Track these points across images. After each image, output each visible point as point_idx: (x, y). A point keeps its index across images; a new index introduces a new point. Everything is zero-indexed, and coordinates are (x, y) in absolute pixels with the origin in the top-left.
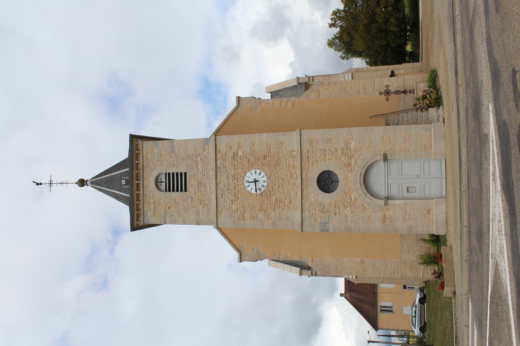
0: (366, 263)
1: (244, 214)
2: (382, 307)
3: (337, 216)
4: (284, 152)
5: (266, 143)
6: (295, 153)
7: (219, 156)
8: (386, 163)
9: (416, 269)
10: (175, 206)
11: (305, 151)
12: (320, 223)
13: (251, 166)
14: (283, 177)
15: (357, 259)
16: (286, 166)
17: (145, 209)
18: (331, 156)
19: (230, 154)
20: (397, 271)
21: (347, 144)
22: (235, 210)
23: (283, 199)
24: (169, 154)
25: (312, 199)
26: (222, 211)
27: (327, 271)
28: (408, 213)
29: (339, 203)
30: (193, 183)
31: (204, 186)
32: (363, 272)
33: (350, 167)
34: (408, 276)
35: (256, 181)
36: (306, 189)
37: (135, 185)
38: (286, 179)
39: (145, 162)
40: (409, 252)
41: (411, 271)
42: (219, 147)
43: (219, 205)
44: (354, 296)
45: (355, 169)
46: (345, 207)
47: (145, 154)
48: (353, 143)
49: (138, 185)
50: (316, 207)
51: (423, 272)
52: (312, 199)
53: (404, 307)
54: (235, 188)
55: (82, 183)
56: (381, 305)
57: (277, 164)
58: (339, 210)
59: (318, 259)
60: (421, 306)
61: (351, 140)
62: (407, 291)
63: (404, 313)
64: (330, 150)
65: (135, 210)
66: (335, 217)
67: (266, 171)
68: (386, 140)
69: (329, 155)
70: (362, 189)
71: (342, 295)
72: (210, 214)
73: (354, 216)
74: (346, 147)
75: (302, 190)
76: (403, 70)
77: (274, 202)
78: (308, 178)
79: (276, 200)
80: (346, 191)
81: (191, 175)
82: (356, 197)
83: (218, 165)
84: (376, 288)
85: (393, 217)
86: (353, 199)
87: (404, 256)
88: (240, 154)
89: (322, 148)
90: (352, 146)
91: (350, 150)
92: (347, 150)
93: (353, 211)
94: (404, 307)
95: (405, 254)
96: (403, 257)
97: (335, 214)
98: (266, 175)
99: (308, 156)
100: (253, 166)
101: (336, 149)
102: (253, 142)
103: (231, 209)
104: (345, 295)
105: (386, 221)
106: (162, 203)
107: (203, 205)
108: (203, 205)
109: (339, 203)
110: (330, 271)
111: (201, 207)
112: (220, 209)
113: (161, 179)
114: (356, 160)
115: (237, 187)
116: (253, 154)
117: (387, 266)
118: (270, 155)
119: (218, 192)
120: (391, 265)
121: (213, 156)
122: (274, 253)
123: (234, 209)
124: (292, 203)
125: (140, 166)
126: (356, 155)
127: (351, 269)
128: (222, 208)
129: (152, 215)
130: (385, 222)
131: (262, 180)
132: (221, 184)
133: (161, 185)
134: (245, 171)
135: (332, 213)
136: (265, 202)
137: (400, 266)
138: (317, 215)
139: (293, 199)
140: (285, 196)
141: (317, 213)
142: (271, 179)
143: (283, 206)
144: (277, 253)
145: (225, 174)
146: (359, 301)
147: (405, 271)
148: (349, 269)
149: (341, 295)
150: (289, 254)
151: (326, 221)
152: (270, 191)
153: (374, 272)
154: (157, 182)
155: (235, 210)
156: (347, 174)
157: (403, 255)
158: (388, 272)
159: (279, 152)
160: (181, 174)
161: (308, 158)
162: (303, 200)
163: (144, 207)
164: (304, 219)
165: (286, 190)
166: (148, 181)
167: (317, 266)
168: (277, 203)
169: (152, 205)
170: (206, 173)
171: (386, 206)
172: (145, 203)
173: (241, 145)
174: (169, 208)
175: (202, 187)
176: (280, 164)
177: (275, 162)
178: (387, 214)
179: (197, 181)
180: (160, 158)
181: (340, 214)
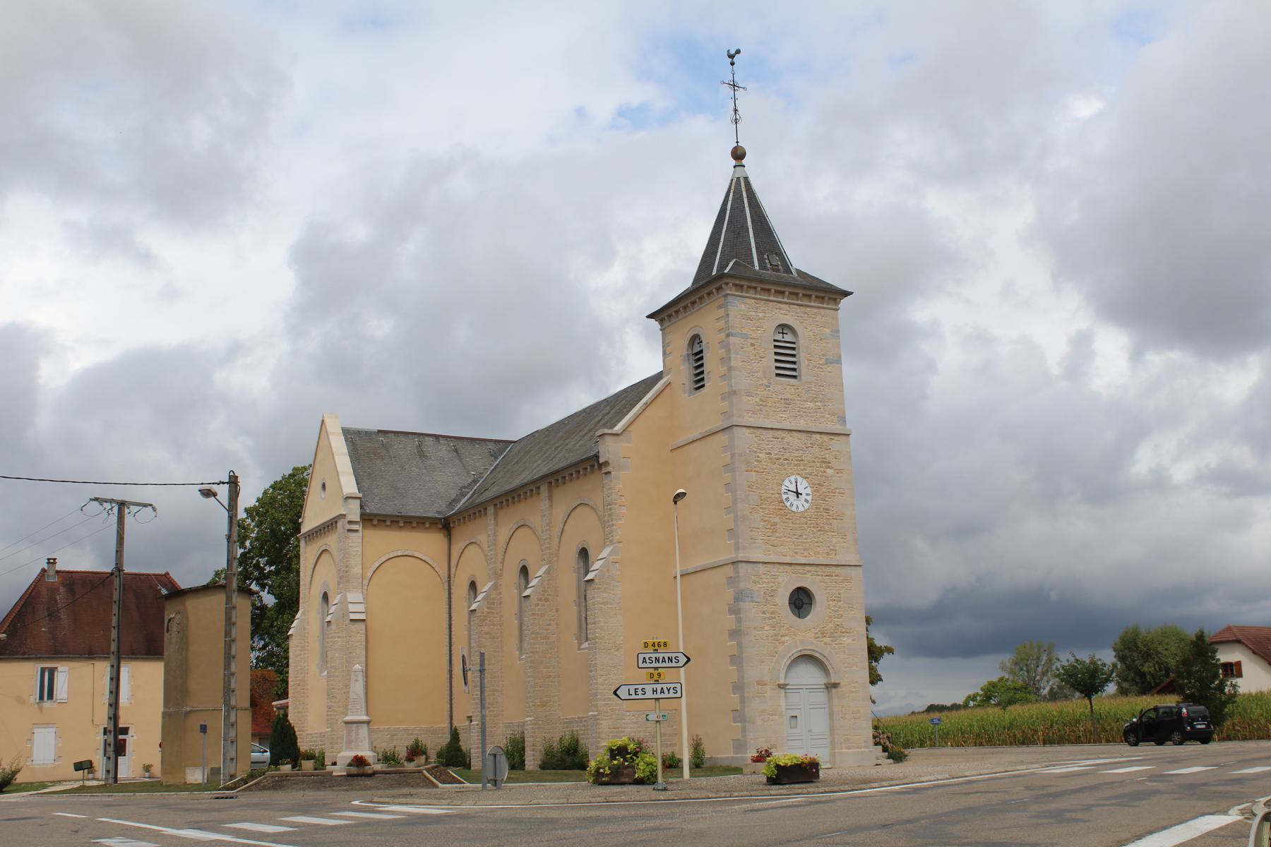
1: (755, 471)
2: (52, 671)
4: (834, 540)
6: (833, 556)
7: (826, 438)
8: (824, 686)
10: (755, 356)
11: (838, 571)
13: (816, 487)
14: (804, 536)
15: (622, 638)
16: (817, 542)
17: (749, 301)
19: (829, 457)
21: (847, 632)
22: (758, 457)
24: (824, 355)
25: (780, 579)
29: (777, 618)
30: (788, 390)
31: (785, 409)
33: (821, 636)
34: (601, 722)
35: (798, 494)
37: (783, 289)
38: (800, 540)
39: (813, 309)
41: (609, 728)
42: (836, 438)
43: (764, 432)
44: (58, 598)
46: (773, 627)
47: (822, 311)
49: (782, 293)
50: (771, 584)
52: (780, 579)
53: (54, 730)
54: (786, 459)
55: (738, 154)
56: (59, 669)
57: (819, 529)
58: (769, 619)
59: (618, 573)
60: (265, 762)
62: (98, 738)
63: (36, 730)
64: (840, 607)
65: (749, 284)
67: (811, 510)
68: (855, 688)
69: (834, 606)
70: (797, 652)
71: (52, 562)
73: (762, 639)
74: (844, 630)
75: (791, 564)
76: (533, 720)
77: (773, 520)
78: (805, 574)
79: (775, 524)
81: (798, 389)
83: (814, 436)
84: (137, 658)
85: (764, 696)
86: (783, 639)
88: (830, 472)
89: (842, 596)
90: (845, 639)
91: (841, 636)
92: (841, 632)
93: (770, 638)
94: (54, 730)
97: (764, 613)
98: (806, 511)
99: (832, 576)
100: (815, 491)
101: (842, 615)
102: (843, 493)
103: (759, 451)
104: (52, 573)
106: (759, 332)
107: (761, 405)
108: (761, 405)
109: (777, 618)
110: (601, 592)
111: (757, 400)
112: (758, 432)
113: (786, 334)
114: (830, 644)
115: (788, 463)
116: (829, 492)
118: (829, 519)
119: (780, 432)
121: (822, 428)
123: (760, 455)
124: (773, 548)
125: (806, 302)
126: (836, 644)
127: (606, 628)
129: (742, 313)
130: (758, 684)
131: (795, 503)
132: (791, 438)
133: (779, 333)
134: (808, 478)
135: (765, 609)
136: (771, 507)
137: (616, 710)
138: (760, 586)
139: (778, 549)
140: (781, 538)
141: (764, 585)
142: (800, 517)
143: (768, 534)
144: (624, 500)
145: (803, 446)
146: (48, 609)
148: (606, 625)
149: (52, 561)
150: (622, 522)
151: (755, 599)
152: (786, 515)
154: (783, 328)
155: (758, 457)
156: (813, 630)
157: (632, 713)
158: (605, 689)
159: (834, 532)
160: (777, 361)
161: (828, 576)
162: (778, 566)
163: (751, 300)
164: (755, 565)
165: (789, 539)
166: (786, 312)
167: (608, 570)
169: (754, 313)
170: (802, 413)
172: (756, 301)
173: (840, 475)
174: (752, 345)
176: (819, 533)
178: (768, 687)
179: (792, 397)
180: (818, 337)
181: (764, 619)
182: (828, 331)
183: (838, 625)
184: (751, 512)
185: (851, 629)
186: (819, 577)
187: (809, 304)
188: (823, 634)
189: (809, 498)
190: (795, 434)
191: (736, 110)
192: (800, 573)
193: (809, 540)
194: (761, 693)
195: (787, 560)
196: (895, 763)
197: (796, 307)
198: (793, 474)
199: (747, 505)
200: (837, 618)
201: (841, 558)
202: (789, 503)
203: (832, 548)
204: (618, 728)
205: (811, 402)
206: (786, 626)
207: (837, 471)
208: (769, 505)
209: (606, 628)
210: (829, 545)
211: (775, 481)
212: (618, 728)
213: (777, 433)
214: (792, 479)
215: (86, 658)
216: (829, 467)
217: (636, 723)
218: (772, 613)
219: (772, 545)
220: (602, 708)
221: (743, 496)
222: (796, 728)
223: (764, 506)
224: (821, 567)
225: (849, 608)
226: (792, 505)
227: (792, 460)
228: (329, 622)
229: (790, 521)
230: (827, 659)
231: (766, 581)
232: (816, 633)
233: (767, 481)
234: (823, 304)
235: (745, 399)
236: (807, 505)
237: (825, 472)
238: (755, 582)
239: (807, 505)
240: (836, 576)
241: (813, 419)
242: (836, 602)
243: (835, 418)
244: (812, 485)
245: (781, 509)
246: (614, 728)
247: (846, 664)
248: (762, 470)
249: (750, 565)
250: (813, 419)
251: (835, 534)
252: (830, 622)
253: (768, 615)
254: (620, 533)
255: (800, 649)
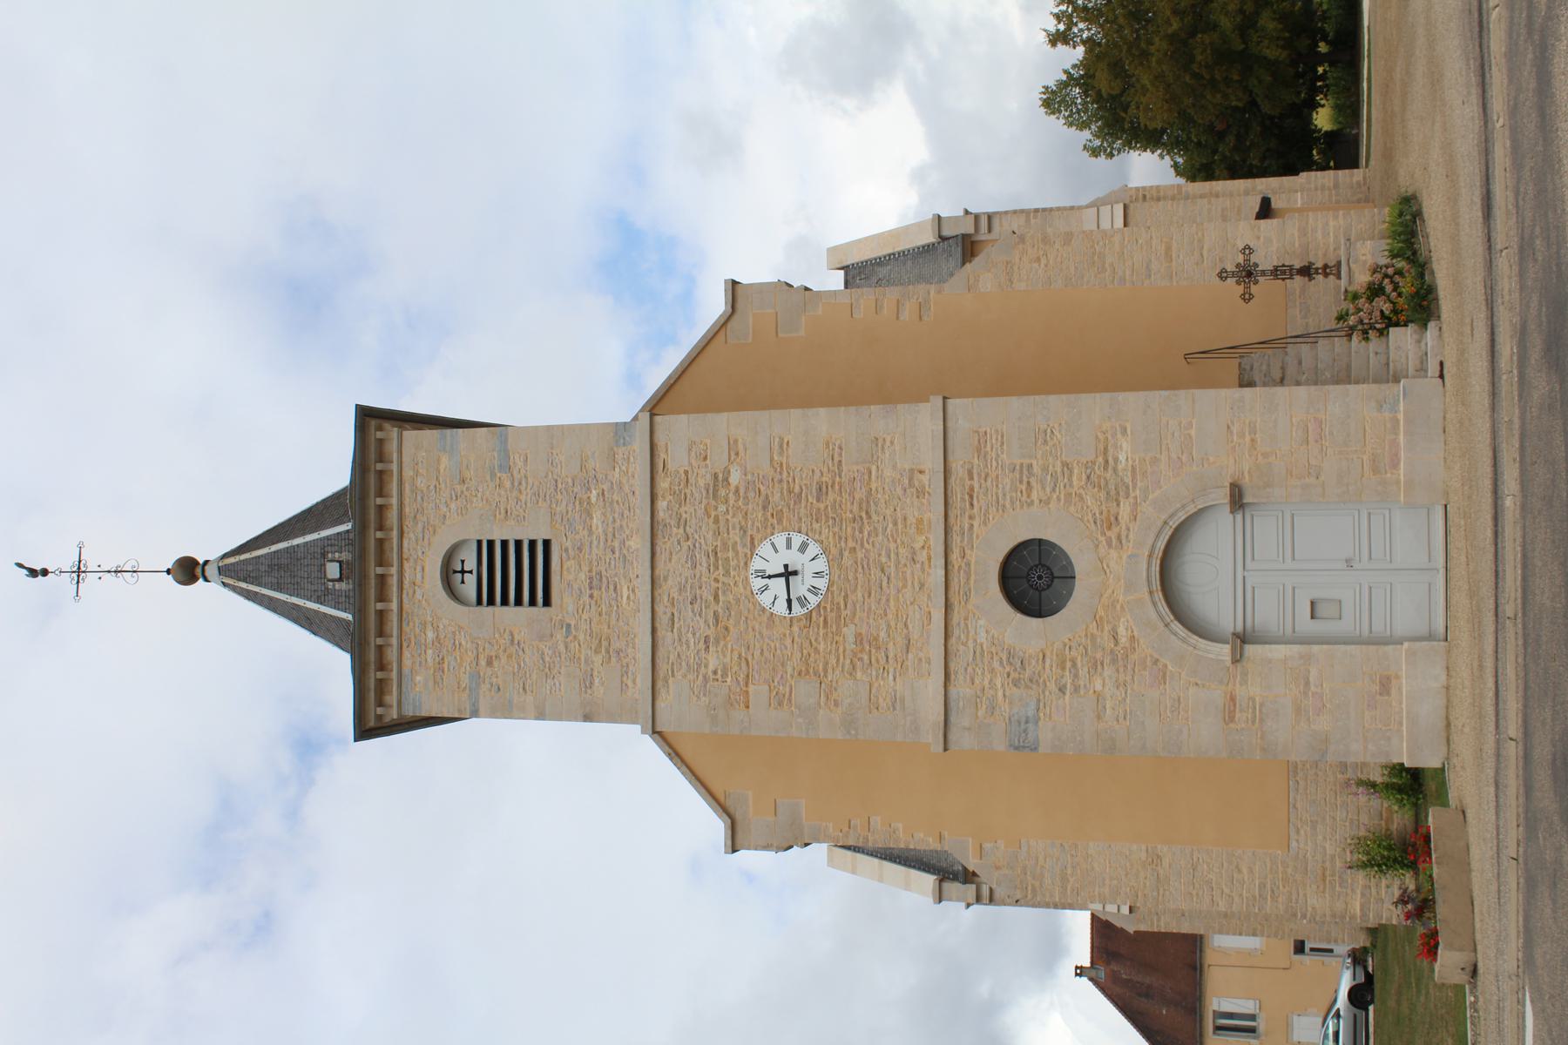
0: (1166, 862)
1: (747, 685)
2: (1228, 643)
3: (1067, 697)
4: (888, 473)
5: (827, 444)
7: (663, 484)
8: (1239, 517)
9: (1340, 886)
10: (510, 656)
12: (1010, 719)
13: (775, 520)
14: (884, 560)
15: (1135, 847)
16: (895, 524)
17: (407, 662)
18: (1048, 490)
19: (703, 479)
20: (1273, 891)
21: (1106, 449)
22: (715, 673)
23: (883, 634)
24: (493, 475)
26: (673, 676)
27: (1029, 888)
28: (1312, 688)
30: (571, 577)
31: (612, 587)
32: (1155, 894)
34: (1310, 909)
36: (963, 603)
37: (373, 582)
38: (893, 569)
39: (407, 501)
40: (1314, 825)
41: (1324, 892)
42: (663, 456)
45: (1131, 536)
46: (1095, 666)
47: (408, 473)
48: (1124, 445)
50: (996, 664)
51: (1363, 895)
53: (1295, 1018)
56: (1216, 1008)
58: (1076, 676)
60: (1355, 1016)
61: (1119, 435)
64: (1045, 469)
65: (372, 667)
66: (1060, 702)
68: (1242, 435)
69: (1043, 488)
70: (1154, 604)
72: (630, 683)
74: (1100, 459)
75: (948, 607)
77: (851, 646)
78: (968, 564)
79: (859, 638)
80: (1101, 613)
81: (566, 550)
82: (1136, 633)
85: (1262, 705)
86: (1123, 640)
87: (1297, 841)
88: (735, 478)
89: (1018, 462)
90: (1122, 457)
91: (1115, 470)
92: (1106, 468)
93: (1121, 679)
94: (1295, 1018)
95: (1302, 832)
96: (1294, 844)
97: (1062, 690)
98: (825, 551)
99: (972, 489)
100: (780, 521)
101: (1065, 465)
105: (1238, 715)
106: (464, 643)
107: (608, 652)
108: (608, 652)
111: (598, 659)
112: (663, 668)
113: (463, 562)
114: (1136, 503)
115: (724, 593)
117: (1240, 871)
118: (840, 484)
119: (660, 609)
120: (1251, 871)
122: (850, 821)
123: (711, 667)
125: (392, 517)
126: (1134, 487)
127: (1115, 882)
128: (673, 664)
129: (431, 683)
130: (1232, 719)
133: (463, 582)
134: (752, 539)
135: (1052, 686)
138: (1000, 693)
139: (915, 636)
140: (889, 626)
142: (840, 567)
143: (882, 661)
145: (685, 548)
147: (1301, 895)
148: (1107, 882)
149: (1078, 971)
151: (1031, 713)
153: (1194, 893)
154: (449, 573)
155: (715, 673)
156: (1103, 550)
158: (1241, 895)
159: (870, 473)
161: (971, 497)
162: (953, 641)
164: (952, 704)
165: (892, 603)
166: (419, 568)
167: (998, 868)
168: (862, 651)
169: (430, 652)
170: (616, 544)
171: (1239, 665)
172: (405, 645)
173: (741, 447)
174: (490, 663)
175: (603, 589)
176: (875, 517)
177: (855, 508)
178: (1241, 693)
179: (585, 568)
180: (458, 488)
181: (1076, 689)
182: (445, 461)
183: (1088, 477)
184: (836, 704)
185: (1097, 437)
186: (976, 523)
187: (395, 507)
188: (1111, 521)
189: (797, 539)
190: (661, 569)
191: (109, 572)
192: (968, 579)
193: (892, 546)
194: (1254, 712)
195: (938, 616)
196: (1439, 317)
197: (405, 542)
198: (746, 581)
199: (821, 712)
200: (1070, 479)
201: (931, 460)
202: (810, 597)
203: (906, 481)
204: (1324, 869)
205: (592, 518)
206: (1093, 627)
207: (733, 457)
208: (817, 651)
209: (1115, 882)
210: (899, 491)
211: (764, 631)
212: (1324, 869)
213: (663, 620)
214: (757, 583)
215: (1201, 975)
216: (726, 480)
217: (1314, 828)
218: (1063, 669)
219: (908, 652)
220: (1280, 906)
221: (800, 720)
222: (1340, 601)
223: (821, 667)
224: (952, 520)
225: (1045, 442)
226: (814, 590)
227: (716, 580)
228: (1131, 910)
229: (852, 597)
230: (1172, 516)
231: (988, 677)
232: (1110, 545)
233: (766, 653)
234: (392, 471)
235: (599, 690)
236: (813, 549)
237: (737, 491)
238: (992, 709)
239: (813, 549)
240: (971, 478)
241: (626, 512)
242: (1033, 481)
243: (621, 452)
244: (768, 531)
245: (825, 621)
246: (1324, 880)
247: (1184, 458)
248: (744, 665)
249: (953, 719)
250: (626, 512)
251: (874, 468)
252: (1081, 498)
253: (1068, 679)
254: (922, 835)
255: (1147, 596)
